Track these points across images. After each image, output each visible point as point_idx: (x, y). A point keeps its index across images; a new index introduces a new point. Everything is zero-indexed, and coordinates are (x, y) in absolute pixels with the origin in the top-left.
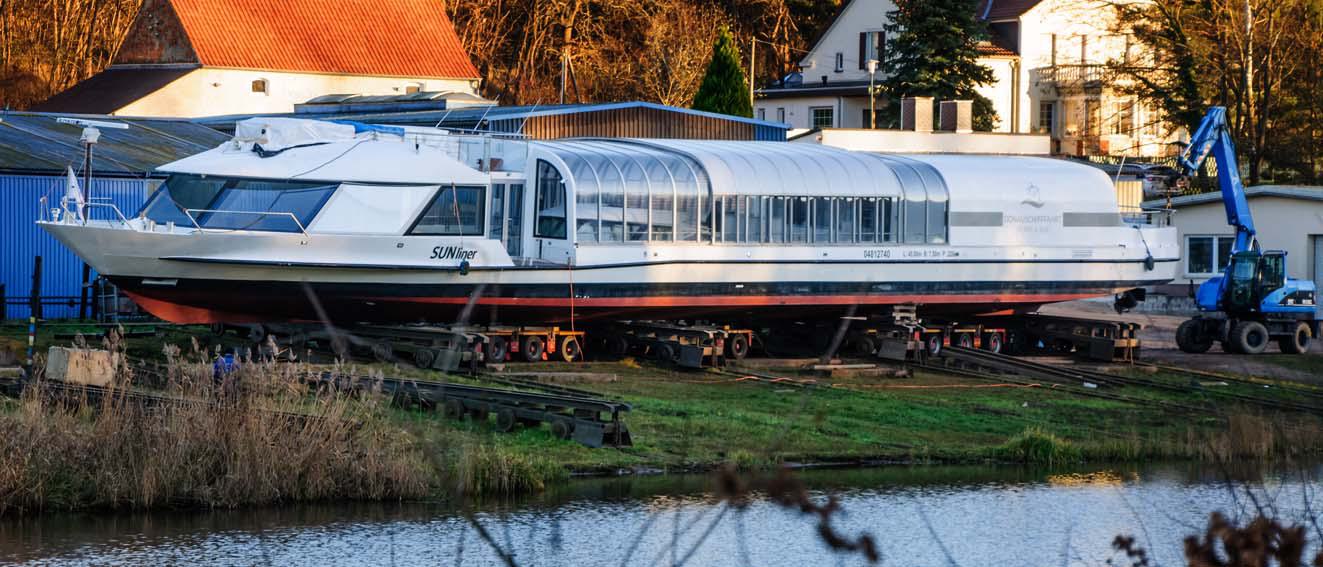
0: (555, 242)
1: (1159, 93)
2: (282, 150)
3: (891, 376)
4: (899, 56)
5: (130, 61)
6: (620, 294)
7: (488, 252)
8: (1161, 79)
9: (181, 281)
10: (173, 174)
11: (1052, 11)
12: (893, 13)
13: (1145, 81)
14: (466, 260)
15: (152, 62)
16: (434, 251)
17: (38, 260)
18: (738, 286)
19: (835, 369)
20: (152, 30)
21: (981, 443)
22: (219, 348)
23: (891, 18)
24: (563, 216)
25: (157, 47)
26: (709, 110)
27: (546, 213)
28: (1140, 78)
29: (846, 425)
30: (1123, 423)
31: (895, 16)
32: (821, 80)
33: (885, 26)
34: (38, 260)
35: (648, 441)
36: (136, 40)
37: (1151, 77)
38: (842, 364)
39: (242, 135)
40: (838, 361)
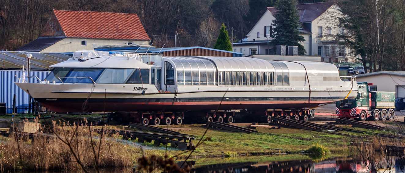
0: (171, 86)
1: (352, 43)
2: (87, 60)
3: (274, 128)
4: (276, 33)
5: (45, 36)
6: (191, 101)
7: (151, 89)
8: (353, 40)
9: (58, 99)
10: (55, 68)
11: (321, 20)
12: (274, 20)
13: (348, 40)
14: (144, 91)
15: (51, 36)
16: (134, 88)
17: (15, 95)
18: (227, 99)
19: (257, 126)
20: (51, 26)
21: (301, 148)
22: (68, 122)
23: (273, 22)
24: (173, 79)
25: (53, 32)
26: (219, 49)
27: (168, 79)
28: (347, 40)
29: (261, 143)
30: (342, 142)
31: (275, 21)
32: (253, 40)
33: (272, 24)
34: (15, 95)
35: (200, 149)
36: (47, 30)
37: (350, 39)
38: (259, 125)
39: (75, 56)
40: (258, 124)
